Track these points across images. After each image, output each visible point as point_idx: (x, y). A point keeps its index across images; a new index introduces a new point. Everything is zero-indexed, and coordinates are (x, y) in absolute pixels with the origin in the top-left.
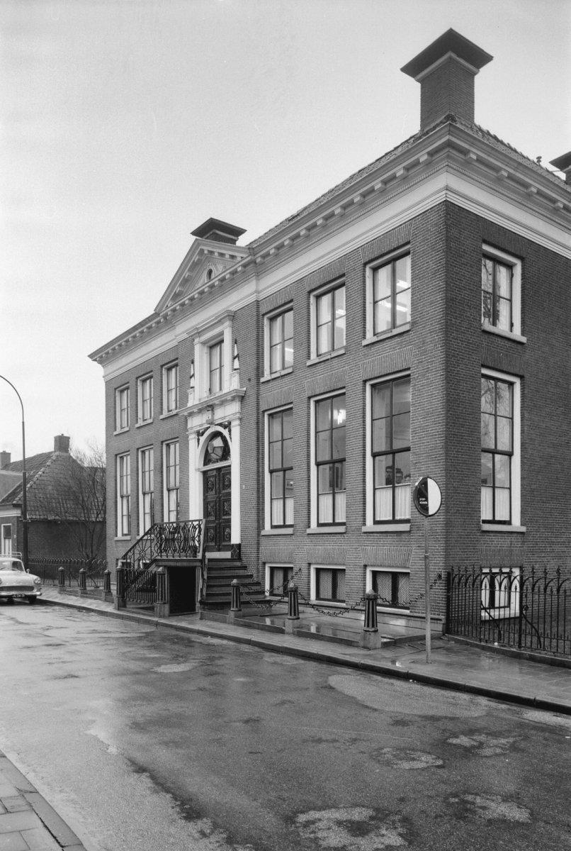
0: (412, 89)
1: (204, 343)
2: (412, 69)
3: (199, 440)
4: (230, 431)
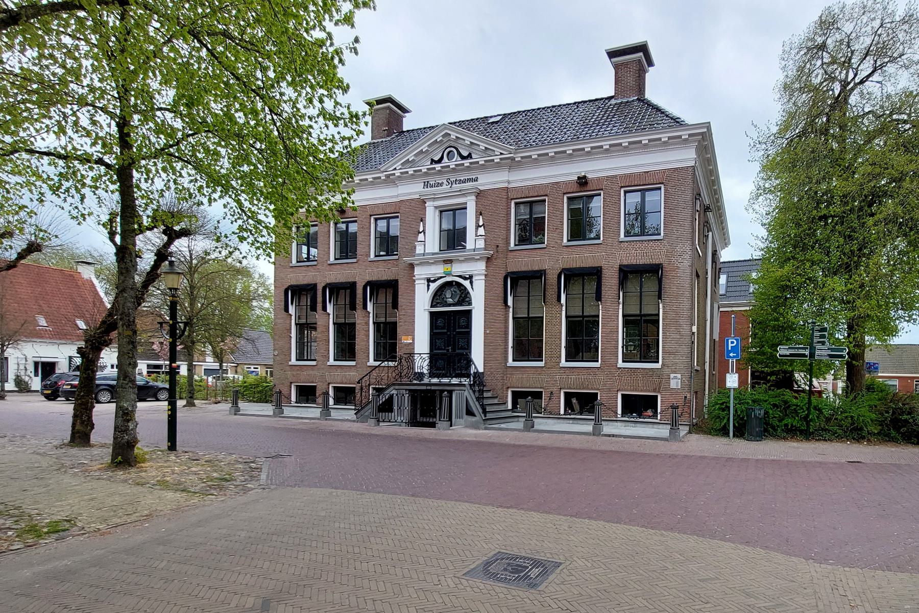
2: (612, 54)
3: (428, 286)
4: (471, 283)
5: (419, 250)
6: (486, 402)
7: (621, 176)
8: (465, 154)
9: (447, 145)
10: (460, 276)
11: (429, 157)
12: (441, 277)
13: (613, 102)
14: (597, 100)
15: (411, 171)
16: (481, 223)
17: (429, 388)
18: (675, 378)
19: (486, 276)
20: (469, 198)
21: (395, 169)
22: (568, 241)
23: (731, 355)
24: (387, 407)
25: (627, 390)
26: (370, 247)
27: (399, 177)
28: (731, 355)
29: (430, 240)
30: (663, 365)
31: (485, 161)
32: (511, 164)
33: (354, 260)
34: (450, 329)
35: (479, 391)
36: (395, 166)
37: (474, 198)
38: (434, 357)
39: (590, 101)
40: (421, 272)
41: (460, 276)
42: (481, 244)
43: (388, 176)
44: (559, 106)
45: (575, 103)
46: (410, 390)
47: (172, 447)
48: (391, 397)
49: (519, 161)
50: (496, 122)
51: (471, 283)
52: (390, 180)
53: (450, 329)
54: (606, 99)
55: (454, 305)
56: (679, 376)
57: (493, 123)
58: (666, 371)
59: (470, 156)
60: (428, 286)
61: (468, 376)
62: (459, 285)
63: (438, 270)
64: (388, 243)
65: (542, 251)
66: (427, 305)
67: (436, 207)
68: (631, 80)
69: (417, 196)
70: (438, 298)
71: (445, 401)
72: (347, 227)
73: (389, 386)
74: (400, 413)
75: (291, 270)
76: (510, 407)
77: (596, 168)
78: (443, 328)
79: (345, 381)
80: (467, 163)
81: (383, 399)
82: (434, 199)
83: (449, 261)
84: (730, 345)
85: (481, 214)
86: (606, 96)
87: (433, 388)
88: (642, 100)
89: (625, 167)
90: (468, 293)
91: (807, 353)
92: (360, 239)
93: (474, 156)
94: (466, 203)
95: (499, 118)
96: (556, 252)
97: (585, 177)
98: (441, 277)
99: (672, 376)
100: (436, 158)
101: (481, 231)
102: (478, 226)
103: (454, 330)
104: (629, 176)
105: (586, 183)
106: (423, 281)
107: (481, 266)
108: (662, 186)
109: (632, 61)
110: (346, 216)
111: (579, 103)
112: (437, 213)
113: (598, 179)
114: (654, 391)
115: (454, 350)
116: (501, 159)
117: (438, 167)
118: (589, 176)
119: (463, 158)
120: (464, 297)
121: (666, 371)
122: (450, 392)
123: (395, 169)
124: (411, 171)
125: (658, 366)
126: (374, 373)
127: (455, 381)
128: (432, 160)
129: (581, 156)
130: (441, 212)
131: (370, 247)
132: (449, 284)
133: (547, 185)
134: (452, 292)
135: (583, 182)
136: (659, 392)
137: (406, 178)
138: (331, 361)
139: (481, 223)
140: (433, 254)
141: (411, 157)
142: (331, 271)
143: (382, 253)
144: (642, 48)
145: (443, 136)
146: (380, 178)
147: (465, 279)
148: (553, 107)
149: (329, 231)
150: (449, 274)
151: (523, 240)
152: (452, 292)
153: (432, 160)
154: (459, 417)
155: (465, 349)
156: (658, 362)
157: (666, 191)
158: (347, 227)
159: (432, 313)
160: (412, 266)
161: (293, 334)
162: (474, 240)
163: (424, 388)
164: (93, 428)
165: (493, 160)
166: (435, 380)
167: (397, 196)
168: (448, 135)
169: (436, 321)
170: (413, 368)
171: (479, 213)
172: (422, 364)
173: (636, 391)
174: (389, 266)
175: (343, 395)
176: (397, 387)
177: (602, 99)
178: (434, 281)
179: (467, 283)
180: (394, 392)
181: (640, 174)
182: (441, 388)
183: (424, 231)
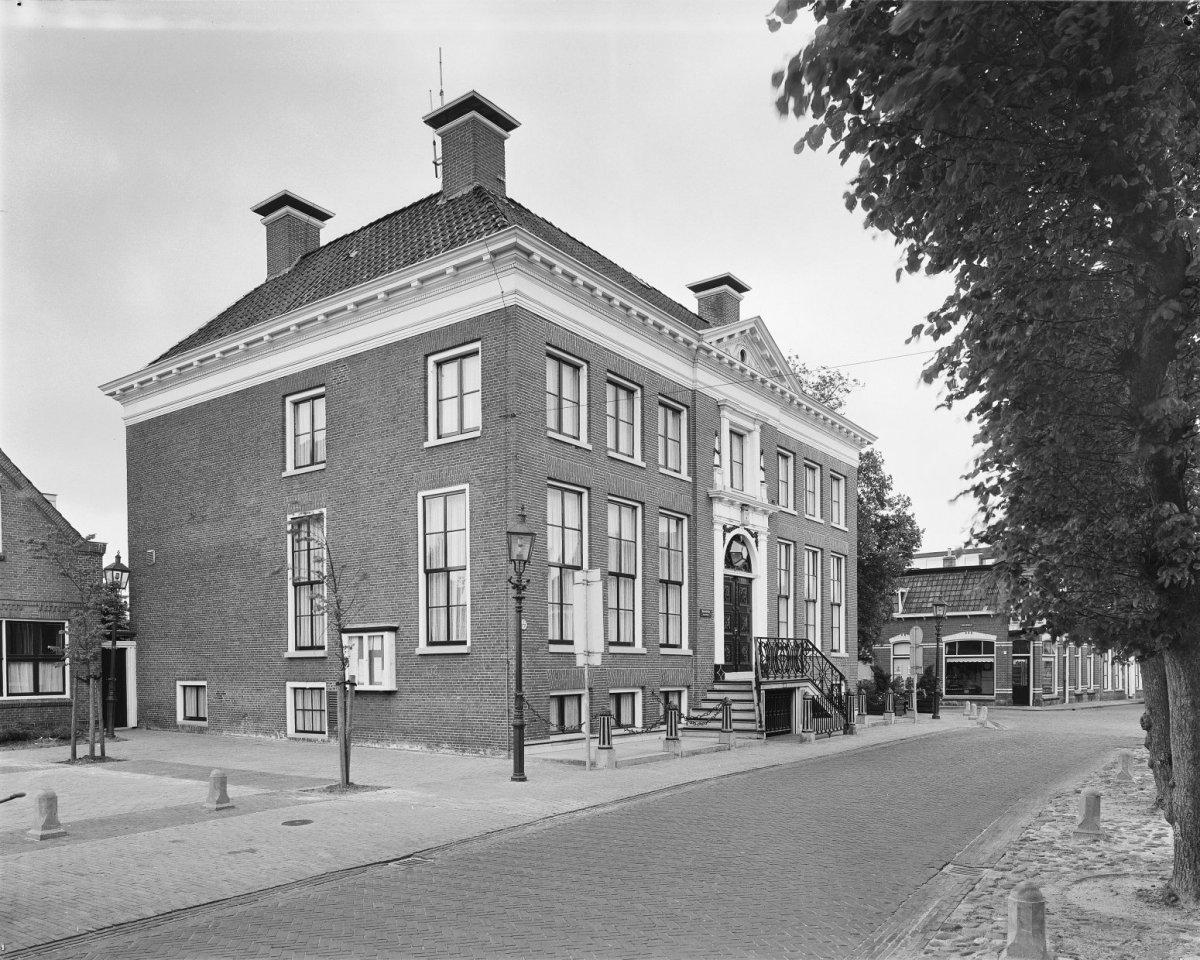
0: (258, 227)
2: (435, 121)
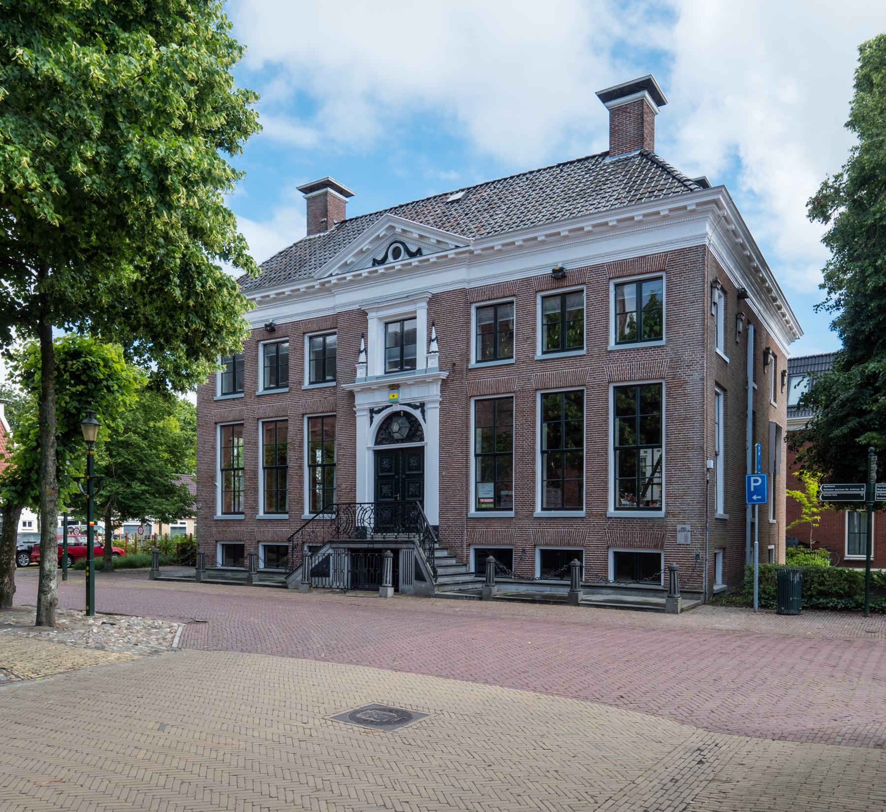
1: (380, 319)
2: (606, 97)
3: (372, 418)
4: (423, 412)
5: (360, 373)
6: (436, 562)
7: (609, 265)
8: (413, 249)
9: (388, 243)
10: (409, 405)
11: (371, 257)
12: (387, 407)
13: (608, 160)
14: (587, 159)
15: (349, 276)
16: (434, 336)
17: (371, 546)
18: (683, 530)
19: (441, 403)
20: (418, 305)
21: (331, 275)
22: (544, 353)
23: (755, 497)
24: (321, 571)
25: (619, 547)
26: (606, 329)
27: (336, 284)
28: (755, 497)
29: (374, 361)
30: (667, 513)
31: (438, 258)
32: (472, 259)
33: (286, 390)
34: (399, 472)
35: (430, 549)
36: (332, 269)
37: (424, 304)
38: (379, 505)
39: (579, 161)
40: (363, 402)
41: (409, 405)
42: (434, 363)
43: (323, 284)
44: (539, 171)
45: (559, 165)
46: (349, 549)
47: (89, 613)
48: (327, 560)
49: (479, 255)
50: (457, 201)
51: (423, 412)
52: (326, 289)
53: (399, 472)
54: (600, 156)
55: (402, 441)
56: (688, 527)
57: (452, 202)
58: (671, 520)
59: (419, 252)
60: (372, 418)
61: (418, 532)
62: (407, 415)
63: (381, 398)
64: (325, 365)
65: (510, 369)
66: (371, 444)
67: (380, 319)
68: (631, 128)
69: (356, 307)
70: (384, 433)
71: (389, 563)
72: (324, 340)
73: (324, 544)
74: (338, 578)
75: (215, 404)
76: (472, 570)
77: (575, 257)
78: (390, 470)
79: (276, 538)
80: (415, 261)
81: (317, 559)
82: (378, 309)
83: (394, 387)
84: (753, 484)
85: (433, 325)
86: (599, 153)
87: (377, 546)
88: (649, 158)
89: (493, 277)
90: (420, 425)
91: (863, 492)
92: (292, 363)
93: (424, 252)
94: (415, 312)
95: (460, 195)
96: (533, 368)
97: (561, 269)
98: (387, 407)
99: (679, 527)
100: (379, 258)
101: (434, 346)
102: (430, 341)
103: (403, 473)
104: (310, 321)
105: (564, 277)
106: (365, 413)
107: (435, 391)
108: (664, 274)
109: (633, 104)
110: (276, 335)
111: (564, 164)
112: (382, 326)
113: (580, 270)
114: (656, 547)
115: (403, 497)
116: (456, 254)
117: (381, 269)
118: (568, 267)
119: (412, 255)
120: (415, 431)
121: (671, 520)
122: (396, 552)
123: (331, 275)
124: (349, 276)
125: (661, 514)
126: (307, 529)
127: (403, 537)
128: (374, 260)
129: (558, 241)
130: (387, 324)
131: (304, 371)
132: (396, 414)
133: (515, 282)
134: (399, 427)
135: (559, 275)
136: (662, 548)
137: (375, 278)
138: (538, 511)
139: (434, 336)
140: (377, 378)
141: (350, 259)
142: (259, 403)
143: (272, 386)
144: (647, 85)
145: (387, 229)
146: (313, 287)
147: (415, 407)
148: (531, 173)
149: (257, 355)
150: (396, 402)
151: (554, 344)
152: (399, 427)
153: (374, 260)
154: (408, 582)
155: (416, 496)
156: (582, 509)
157: (668, 281)
158: (563, 305)
159: (377, 453)
160: (351, 395)
161: (219, 483)
162: (427, 358)
163: (365, 546)
164: (14, 591)
165: (446, 256)
166: (379, 537)
167: (334, 308)
168: (393, 228)
169: (382, 462)
170: (353, 522)
171: (432, 324)
172: (366, 518)
173: (632, 546)
174: (326, 395)
175: (274, 556)
176: (334, 546)
177: (593, 157)
178: (379, 411)
179: (417, 413)
180: (331, 551)
181: (634, 261)
182: (385, 546)
183: (366, 350)
